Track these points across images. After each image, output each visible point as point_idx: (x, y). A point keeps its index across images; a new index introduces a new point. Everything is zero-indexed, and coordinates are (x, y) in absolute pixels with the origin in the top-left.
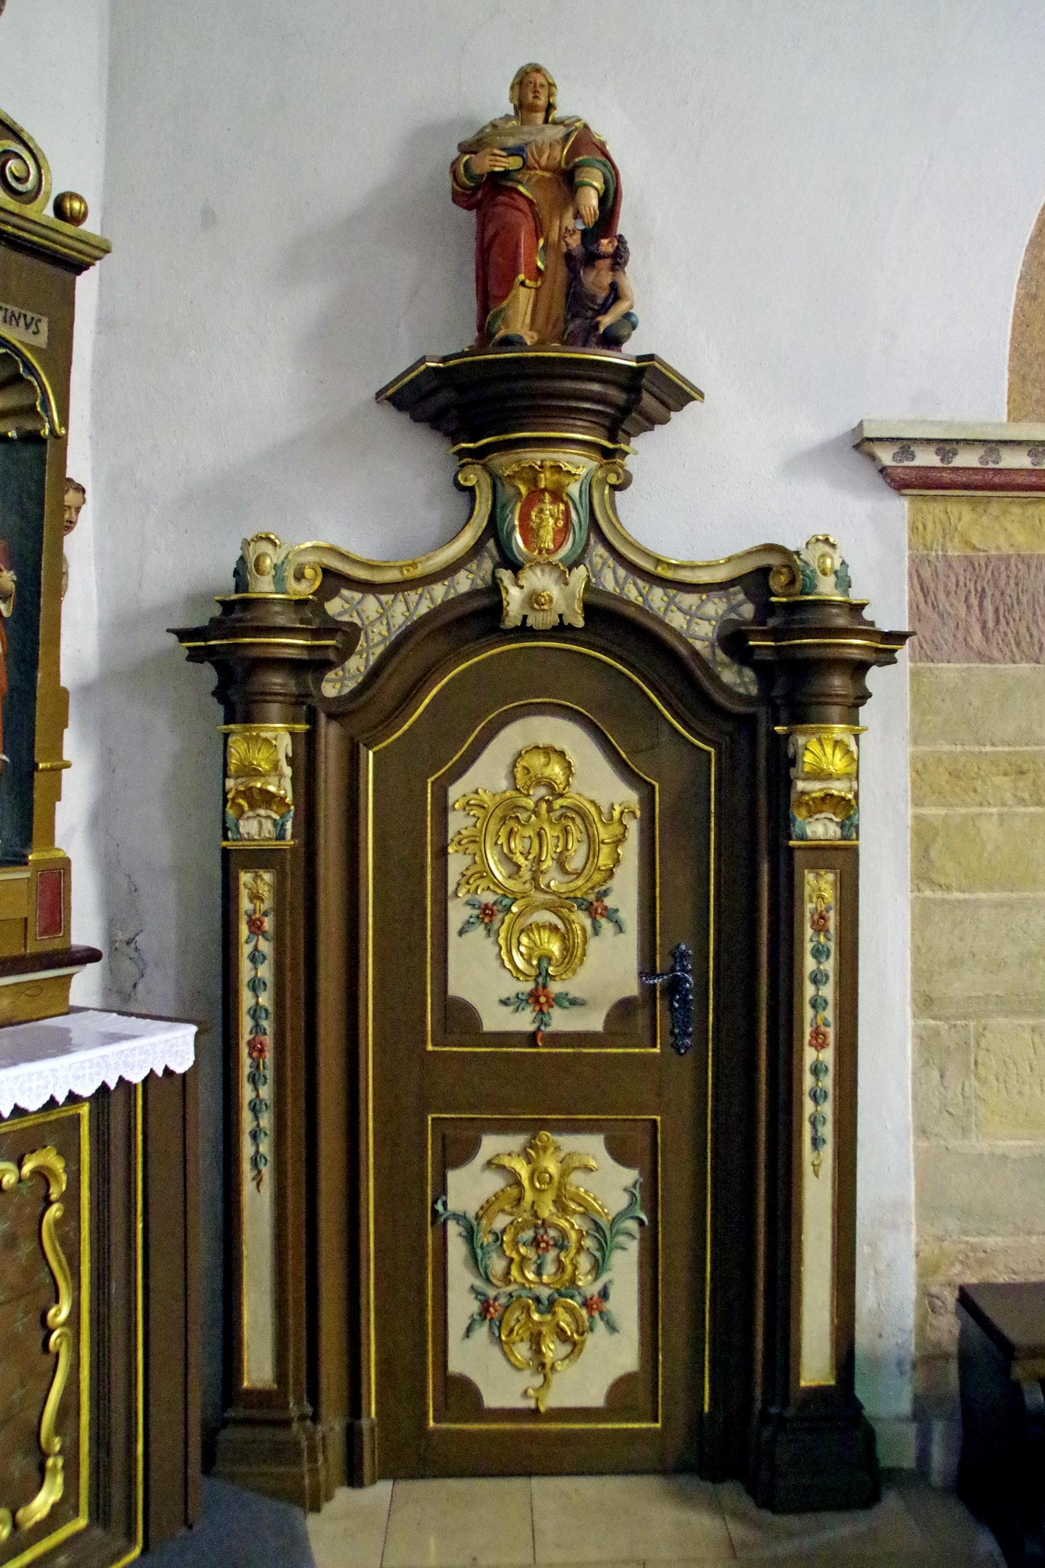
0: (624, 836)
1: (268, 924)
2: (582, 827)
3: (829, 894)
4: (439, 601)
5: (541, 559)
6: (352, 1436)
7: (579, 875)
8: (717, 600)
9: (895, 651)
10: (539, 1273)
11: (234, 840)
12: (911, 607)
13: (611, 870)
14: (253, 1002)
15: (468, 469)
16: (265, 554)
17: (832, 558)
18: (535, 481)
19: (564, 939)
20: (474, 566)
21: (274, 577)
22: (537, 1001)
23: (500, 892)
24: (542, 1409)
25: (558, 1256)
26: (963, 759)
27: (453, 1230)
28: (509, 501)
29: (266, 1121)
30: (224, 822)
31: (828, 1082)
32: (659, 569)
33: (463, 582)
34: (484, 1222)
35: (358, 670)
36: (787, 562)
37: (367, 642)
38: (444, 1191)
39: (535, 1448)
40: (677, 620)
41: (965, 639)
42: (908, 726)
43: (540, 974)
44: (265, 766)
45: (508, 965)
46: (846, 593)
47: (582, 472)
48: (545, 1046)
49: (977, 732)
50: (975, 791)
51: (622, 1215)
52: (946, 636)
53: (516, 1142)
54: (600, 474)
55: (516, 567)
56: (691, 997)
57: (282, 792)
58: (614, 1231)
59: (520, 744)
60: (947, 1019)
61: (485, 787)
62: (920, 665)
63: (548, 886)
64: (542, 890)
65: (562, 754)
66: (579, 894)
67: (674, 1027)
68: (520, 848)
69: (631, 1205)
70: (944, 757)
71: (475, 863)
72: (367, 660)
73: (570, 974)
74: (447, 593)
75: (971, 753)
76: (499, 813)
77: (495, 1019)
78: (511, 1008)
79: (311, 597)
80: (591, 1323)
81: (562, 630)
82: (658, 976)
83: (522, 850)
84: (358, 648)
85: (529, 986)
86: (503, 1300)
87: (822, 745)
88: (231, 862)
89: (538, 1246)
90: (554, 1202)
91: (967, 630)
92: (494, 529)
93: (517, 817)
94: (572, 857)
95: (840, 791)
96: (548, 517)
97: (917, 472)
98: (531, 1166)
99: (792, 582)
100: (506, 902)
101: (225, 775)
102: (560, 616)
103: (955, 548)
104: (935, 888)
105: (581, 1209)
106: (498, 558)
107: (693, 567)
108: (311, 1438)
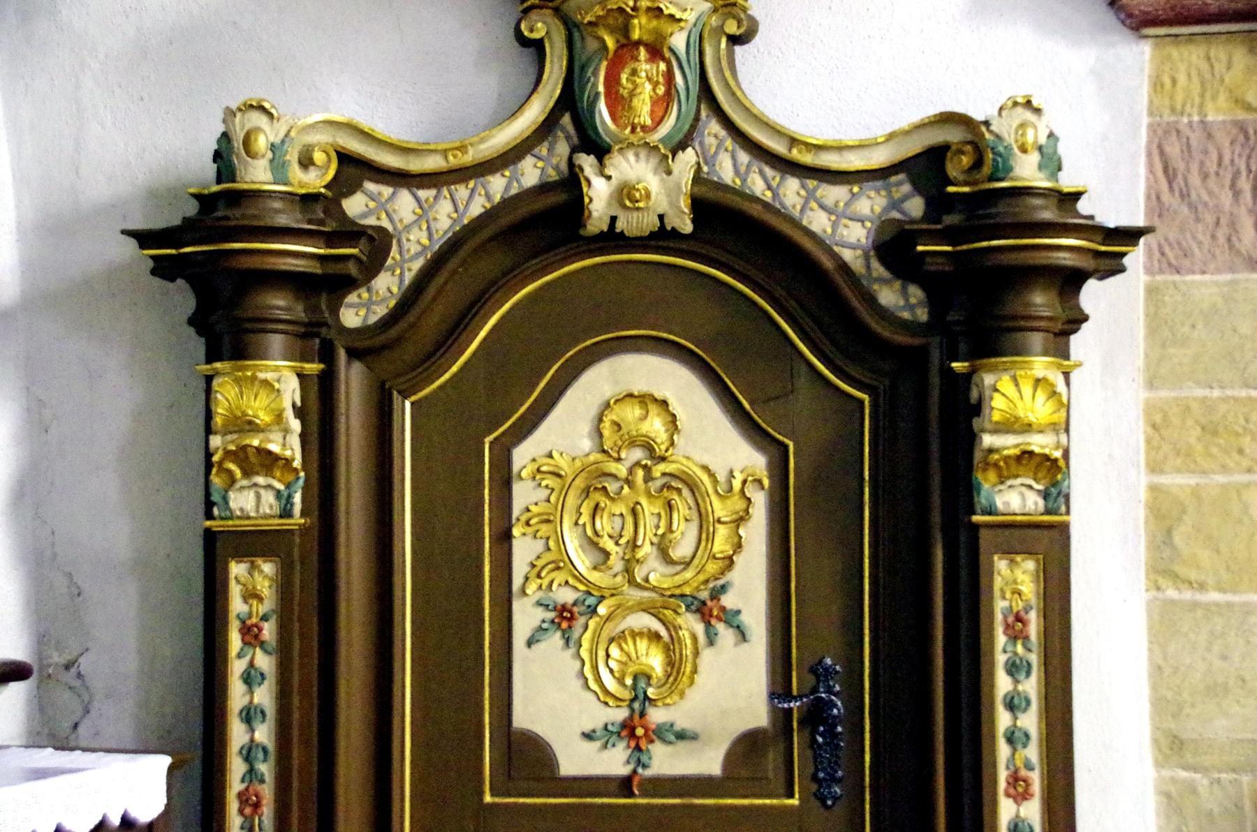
0: (748, 513)
1: (269, 631)
2: (691, 501)
4: (497, 198)
5: (633, 139)
7: (687, 564)
8: (872, 194)
9: (1123, 254)
11: (222, 519)
12: (1148, 197)
13: (730, 558)
14: (246, 739)
15: (534, 15)
16: (258, 130)
17: (1035, 127)
18: (625, 30)
20: (543, 150)
21: (271, 161)
22: (632, 735)
23: (582, 588)
26: (1223, 407)
28: (589, 60)
30: (208, 494)
32: (795, 151)
33: (530, 173)
35: (389, 290)
36: (969, 137)
37: (401, 253)
40: (818, 222)
41: (1229, 240)
42: (1140, 362)
43: (635, 698)
44: (264, 418)
45: (593, 685)
46: (1054, 176)
47: (690, 16)
48: (645, 794)
49: (1245, 369)
50: (1241, 451)
52: (1200, 236)
54: (714, 21)
55: (600, 151)
56: (839, 729)
57: (288, 453)
59: (608, 391)
61: (562, 449)
62: (1159, 278)
63: (647, 580)
64: (639, 586)
65: (664, 403)
66: (687, 590)
67: (817, 770)
68: (608, 529)
70: (1194, 405)
71: (549, 549)
72: (402, 274)
73: (675, 697)
74: (507, 188)
75: (1236, 399)
76: (580, 483)
77: (577, 759)
78: (598, 744)
79: (323, 190)
81: (663, 237)
82: (795, 698)
83: (611, 531)
84: (389, 262)
85: (621, 714)
87: (1017, 385)
88: (218, 548)
91: (1233, 225)
92: (571, 101)
93: (604, 488)
94: (678, 543)
95: (1043, 447)
96: (643, 83)
99: (978, 164)
100: (591, 601)
101: (209, 431)
102: (661, 217)
103: (1218, 110)
104: (1181, 586)
106: (576, 140)
107: (841, 148)
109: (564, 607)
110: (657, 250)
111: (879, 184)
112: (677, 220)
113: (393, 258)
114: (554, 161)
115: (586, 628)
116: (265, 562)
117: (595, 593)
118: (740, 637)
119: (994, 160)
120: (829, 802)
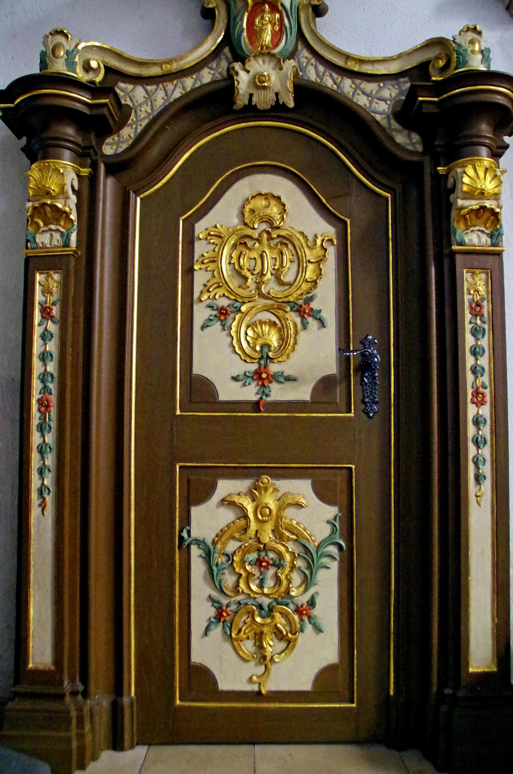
1: (56, 311)
4: (189, 89)
6: (116, 711)
8: (391, 87)
10: (261, 586)
11: (32, 248)
14: (42, 370)
19: (280, 331)
20: (214, 65)
21: (66, 60)
22: (260, 378)
24: (264, 692)
25: (276, 573)
27: (195, 551)
28: (238, 13)
29: (50, 460)
31: (486, 431)
33: (206, 76)
34: (219, 546)
35: (130, 136)
37: (136, 118)
38: (188, 522)
39: (259, 721)
40: (362, 101)
44: (54, 188)
53: (243, 485)
56: (377, 374)
57: (67, 209)
58: (319, 553)
59: (248, 193)
63: (269, 293)
65: (278, 198)
66: (291, 299)
68: (247, 265)
69: (333, 532)
71: (214, 277)
72: (136, 129)
74: (194, 84)
77: (228, 391)
78: (240, 383)
80: (301, 626)
81: (278, 110)
83: (248, 267)
85: (254, 367)
86: (233, 607)
88: (33, 264)
89: (260, 565)
98: (255, 503)
102: (277, 94)
105: (294, 537)
107: (373, 62)
108: (80, 710)
109: (222, 308)
111: (394, 82)
112: (285, 96)
113: (132, 120)
114: (220, 70)
115: (234, 319)
116: (55, 273)
117: (240, 300)
118: (321, 324)
119: (457, 58)
120: (371, 415)
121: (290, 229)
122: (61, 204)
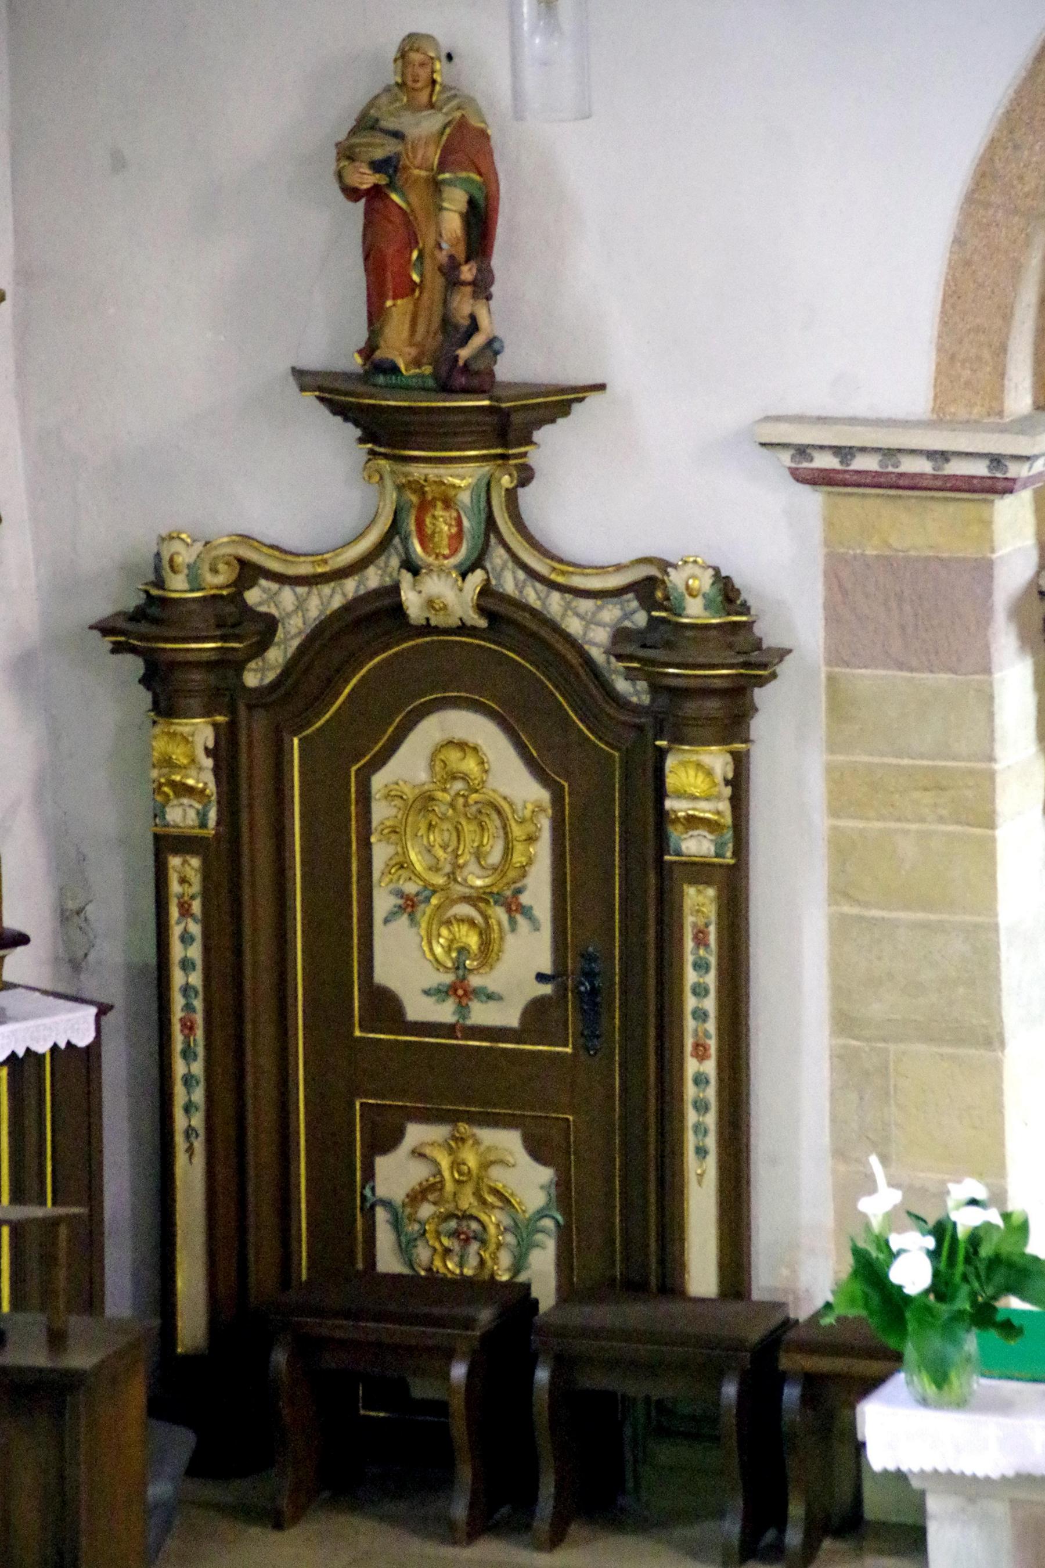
1: (196, 906)
3: (711, 911)
4: (350, 595)
14: (186, 1125)
20: (381, 561)
23: (421, 883)
27: (381, 1215)
40: (574, 626)
51: (541, 1214)
53: (438, 1132)
59: (438, 737)
60: (868, 1040)
63: (465, 880)
65: (475, 749)
66: (495, 890)
72: (285, 652)
74: (285, 652)
77: (419, 1008)
84: (276, 639)
85: (448, 978)
88: (167, 844)
90: (474, 1194)
97: (835, 471)
102: (461, 619)
110: (460, 635)
111: (615, 600)
121: (491, 793)
122: (193, 778)
